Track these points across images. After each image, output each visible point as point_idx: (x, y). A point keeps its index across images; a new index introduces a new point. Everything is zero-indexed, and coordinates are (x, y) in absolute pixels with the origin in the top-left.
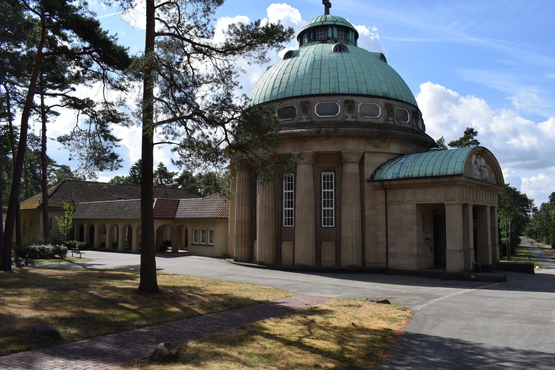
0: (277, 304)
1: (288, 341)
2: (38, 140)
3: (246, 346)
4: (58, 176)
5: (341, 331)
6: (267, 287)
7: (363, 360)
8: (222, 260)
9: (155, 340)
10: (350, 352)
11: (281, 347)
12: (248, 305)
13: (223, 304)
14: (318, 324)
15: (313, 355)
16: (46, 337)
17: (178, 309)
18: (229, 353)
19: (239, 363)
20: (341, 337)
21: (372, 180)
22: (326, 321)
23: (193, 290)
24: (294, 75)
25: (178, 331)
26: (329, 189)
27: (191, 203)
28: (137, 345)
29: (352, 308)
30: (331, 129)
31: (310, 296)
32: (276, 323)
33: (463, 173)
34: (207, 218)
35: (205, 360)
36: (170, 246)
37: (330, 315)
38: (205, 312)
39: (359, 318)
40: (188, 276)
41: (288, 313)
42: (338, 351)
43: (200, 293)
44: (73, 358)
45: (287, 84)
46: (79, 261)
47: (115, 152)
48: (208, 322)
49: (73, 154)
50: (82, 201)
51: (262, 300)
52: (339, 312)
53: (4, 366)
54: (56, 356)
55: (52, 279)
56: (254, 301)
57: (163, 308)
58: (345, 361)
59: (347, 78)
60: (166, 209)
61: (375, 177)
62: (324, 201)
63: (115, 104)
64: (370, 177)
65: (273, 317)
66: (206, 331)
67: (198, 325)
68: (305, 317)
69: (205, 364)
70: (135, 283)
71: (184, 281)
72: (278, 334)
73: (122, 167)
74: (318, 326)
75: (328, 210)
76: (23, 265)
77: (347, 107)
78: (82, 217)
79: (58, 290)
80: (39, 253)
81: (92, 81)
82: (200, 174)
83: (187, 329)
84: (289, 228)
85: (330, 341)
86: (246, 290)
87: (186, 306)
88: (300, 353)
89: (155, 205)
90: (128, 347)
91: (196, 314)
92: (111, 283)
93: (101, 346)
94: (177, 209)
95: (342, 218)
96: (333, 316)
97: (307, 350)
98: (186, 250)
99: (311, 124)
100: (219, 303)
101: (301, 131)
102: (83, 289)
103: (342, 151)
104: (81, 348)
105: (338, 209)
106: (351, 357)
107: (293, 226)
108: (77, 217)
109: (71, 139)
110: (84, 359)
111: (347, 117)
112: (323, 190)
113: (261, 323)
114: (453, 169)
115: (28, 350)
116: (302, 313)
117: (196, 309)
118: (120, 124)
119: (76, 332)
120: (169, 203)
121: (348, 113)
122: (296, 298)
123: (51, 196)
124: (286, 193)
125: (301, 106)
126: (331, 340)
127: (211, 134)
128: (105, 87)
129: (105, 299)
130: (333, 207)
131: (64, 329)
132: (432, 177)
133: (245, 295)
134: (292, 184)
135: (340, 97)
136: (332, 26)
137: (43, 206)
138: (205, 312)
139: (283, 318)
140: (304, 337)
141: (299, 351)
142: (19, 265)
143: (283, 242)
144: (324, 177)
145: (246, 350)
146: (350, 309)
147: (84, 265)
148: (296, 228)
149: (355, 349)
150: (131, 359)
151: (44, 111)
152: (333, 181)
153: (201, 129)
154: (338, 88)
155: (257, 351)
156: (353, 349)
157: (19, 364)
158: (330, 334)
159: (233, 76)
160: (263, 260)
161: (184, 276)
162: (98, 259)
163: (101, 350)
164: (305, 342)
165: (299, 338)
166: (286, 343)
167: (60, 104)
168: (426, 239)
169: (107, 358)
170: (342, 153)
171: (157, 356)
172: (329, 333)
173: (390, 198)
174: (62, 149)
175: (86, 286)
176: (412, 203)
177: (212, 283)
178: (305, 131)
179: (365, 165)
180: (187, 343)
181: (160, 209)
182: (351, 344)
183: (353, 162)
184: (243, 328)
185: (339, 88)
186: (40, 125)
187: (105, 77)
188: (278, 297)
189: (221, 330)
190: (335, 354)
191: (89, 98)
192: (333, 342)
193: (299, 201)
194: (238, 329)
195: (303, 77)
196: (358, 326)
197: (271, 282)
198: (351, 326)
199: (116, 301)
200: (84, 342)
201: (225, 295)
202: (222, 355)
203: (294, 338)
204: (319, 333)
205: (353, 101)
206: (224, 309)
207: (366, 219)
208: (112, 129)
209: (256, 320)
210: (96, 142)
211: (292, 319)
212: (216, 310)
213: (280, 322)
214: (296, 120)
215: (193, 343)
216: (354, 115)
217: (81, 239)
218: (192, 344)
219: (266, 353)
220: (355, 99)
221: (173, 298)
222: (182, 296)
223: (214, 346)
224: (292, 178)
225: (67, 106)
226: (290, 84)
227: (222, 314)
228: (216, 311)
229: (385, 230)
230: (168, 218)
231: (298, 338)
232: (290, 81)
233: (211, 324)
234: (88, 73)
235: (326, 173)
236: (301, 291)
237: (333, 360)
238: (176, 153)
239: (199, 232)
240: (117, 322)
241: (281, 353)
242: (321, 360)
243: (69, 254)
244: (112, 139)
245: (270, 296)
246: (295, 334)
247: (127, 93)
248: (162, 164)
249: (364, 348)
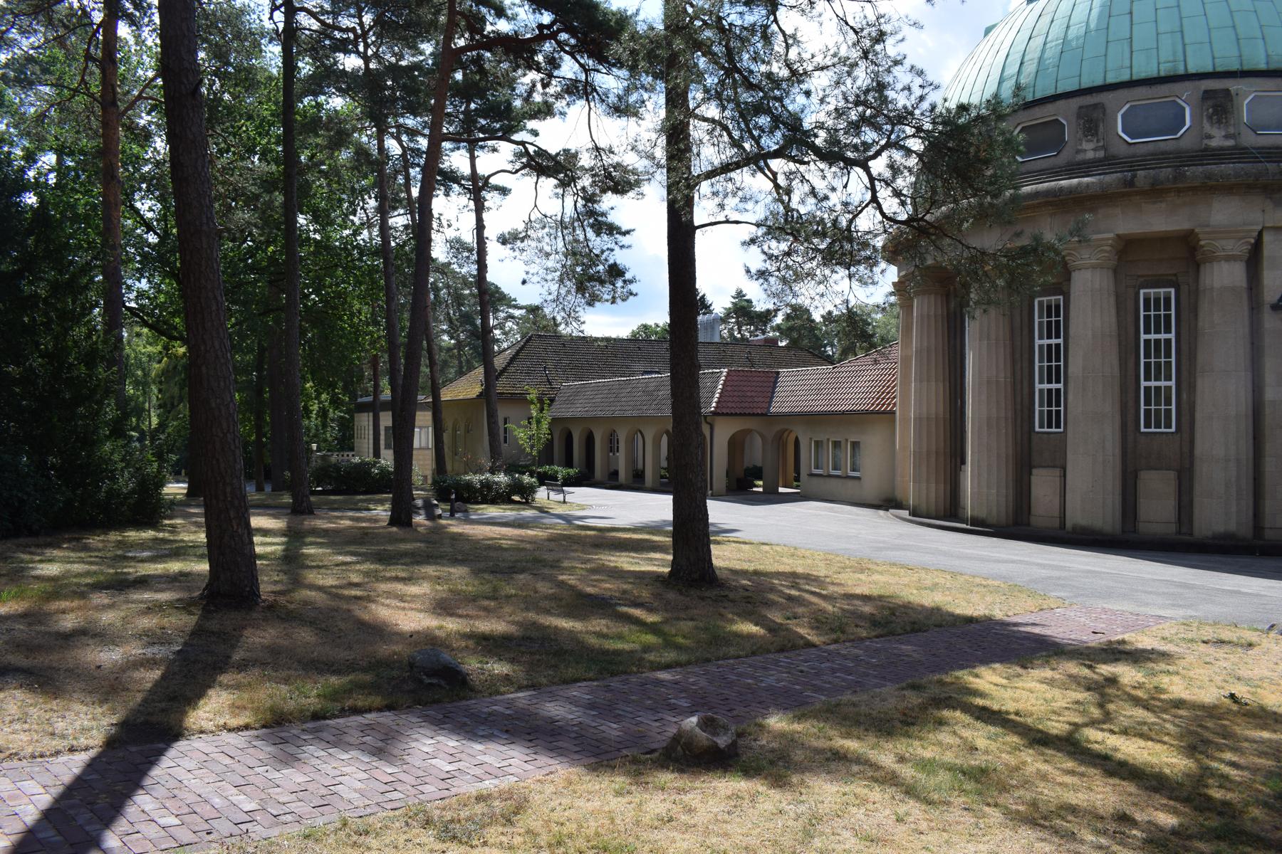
0: (1015, 628)
1: (1040, 735)
2: (470, 250)
3: (921, 739)
4: (520, 328)
5: (1197, 716)
6: (990, 582)
7: (1266, 810)
8: (881, 512)
9: (686, 705)
10: (1224, 781)
11: (1017, 748)
12: (936, 626)
13: (873, 622)
14: (1128, 689)
15: (1112, 781)
16: (434, 681)
17: (758, 628)
18: (873, 755)
19: (894, 788)
20: (1197, 733)
22: (1151, 683)
23: (801, 581)
24: (1057, 40)
25: (749, 684)
27: (806, 377)
28: (641, 713)
29: (1227, 648)
30: (1166, 173)
31: (1105, 611)
32: (1008, 678)
34: (843, 413)
35: (802, 769)
36: (760, 479)
37: (1163, 666)
38: (822, 639)
39: (1250, 679)
40: (796, 549)
41: (1044, 653)
42: (1188, 775)
43: (817, 590)
44: (482, 736)
45: (1039, 63)
46: (560, 510)
47: (618, 262)
48: (828, 664)
49: (531, 271)
50: (567, 381)
51: (976, 614)
52: (1190, 658)
53: (324, 743)
54: (444, 729)
55: (489, 547)
56: (952, 615)
57: (721, 623)
58: (1209, 809)
60: (749, 394)
62: (1147, 318)
63: (616, 150)
65: (1001, 662)
66: (818, 689)
67: (802, 671)
68: (1090, 667)
69: (802, 782)
70: (660, 563)
71: (785, 560)
72: (1012, 710)
73: (636, 295)
74: (1129, 695)
75: (1158, 389)
76: (440, 517)
77: (1211, 110)
78: (569, 415)
79: (492, 572)
80: (480, 490)
81: (564, 102)
82: (830, 313)
83: (771, 681)
85: (1165, 743)
86: (934, 587)
87: (779, 621)
88: (1071, 772)
89: (723, 385)
90: (618, 718)
91: (802, 642)
92: (612, 558)
93: (555, 709)
94: (773, 392)
95: (1198, 408)
96: (1171, 668)
97: (1095, 766)
98: (797, 487)
99: (1107, 163)
100: (861, 616)
101: (1079, 184)
102: (546, 571)
103: (1197, 230)
104: (508, 712)
105: (1187, 384)
106: (1228, 797)
107: (1062, 430)
108: (559, 415)
109: (525, 237)
110: (505, 742)
111: (1210, 137)
112: (1143, 337)
113: (966, 677)
115: (390, 708)
116: (1081, 654)
117: (801, 631)
118: (631, 194)
119: (506, 672)
120: (755, 379)
121: (1212, 124)
122: (1068, 613)
123: (504, 370)
125: (1079, 116)
126: (1166, 739)
127: (833, 189)
128: (592, 113)
129: (590, 595)
130: (1171, 380)
131: (481, 662)
133: (930, 600)
134: (1058, 323)
135: (1187, 84)
137: (487, 395)
138: (822, 639)
139: (1029, 665)
140: (1086, 725)
141: (1070, 764)
142: (431, 516)
143: (1035, 471)
144: (1147, 301)
145: (920, 751)
146: (1220, 652)
147: (567, 519)
148: (1070, 435)
149: (1240, 773)
151: (478, 187)
152: (1173, 312)
153: (808, 181)
154: (1182, 59)
155: (949, 757)
156: (1233, 772)
157: (358, 741)
158: (1165, 720)
159: (890, 41)
160: (982, 513)
161: (786, 549)
162: (600, 506)
163: (552, 721)
164: (1088, 741)
165: (1071, 727)
166: (1034, 739)
167: (509, 167)
169: (560, 744)
170: (1197, 234)
171: (679, 748)
172: (1159, 717)
174: (507, 261)
175: (555, 565)
177: (851, 567)
178: (1093, 183)
179: (1265, 263)
180: (764, 718)
181: (736, 393)
182: (1228, 756)
183: (1230, 258)
184: (915, 687)
185: (1185, 61)
186: (472, 217)
187: (589, 89)
188: (1018, 610)
189: (858, 689)
190: (1178, 783)
191: (569, 150)
192: (1172, 745)
193: (1076, 365)
194: (903, 689)
195: (1081, 41)
196: (1246, 704)
197: (1003, 569)
198: (1228, 701)
199: (613, 602)
200: (519, 698)
201: (880, 598)
202: (851, 761)
203: (1056, 725)
204: (1131, 717)
205: (1227, 92)
206: (874, 634)
208: (612, 208)
209: (952, 669)
210: (577, 241)
211: (1053, 669)
212: (852, 634)
213: (1019, 676)
214: (1066, 156)
215: (781, 720)
216: (1231, 130)
217: (569, 463)
218: (777, 722)
219: (973, 762)
221: (748, 600)
222: (772, 596)
223: (832, 733)
224: (1058, 307)
225: (523, 172)
226: (1047, 62)
227: (867, 646)
228: (852, 637)
230: (754, 415)
231: (1067, 726)
232: (1046, 56)
233: (833, 671)
234: (554, 82)
235: (1152, 291)
236: (1082, 595)
237: (1172, 803)
238: (754, 248)
239: (825, 446)
240: (606, 652)
241: (1017, 769)
242: (1136, 800)
243: (542, 494)
244: (612, 229)
245: (998, 606)
246: (1059, 715)
247: (640, 122)
248: (741, 291)
249: (1270, 774)
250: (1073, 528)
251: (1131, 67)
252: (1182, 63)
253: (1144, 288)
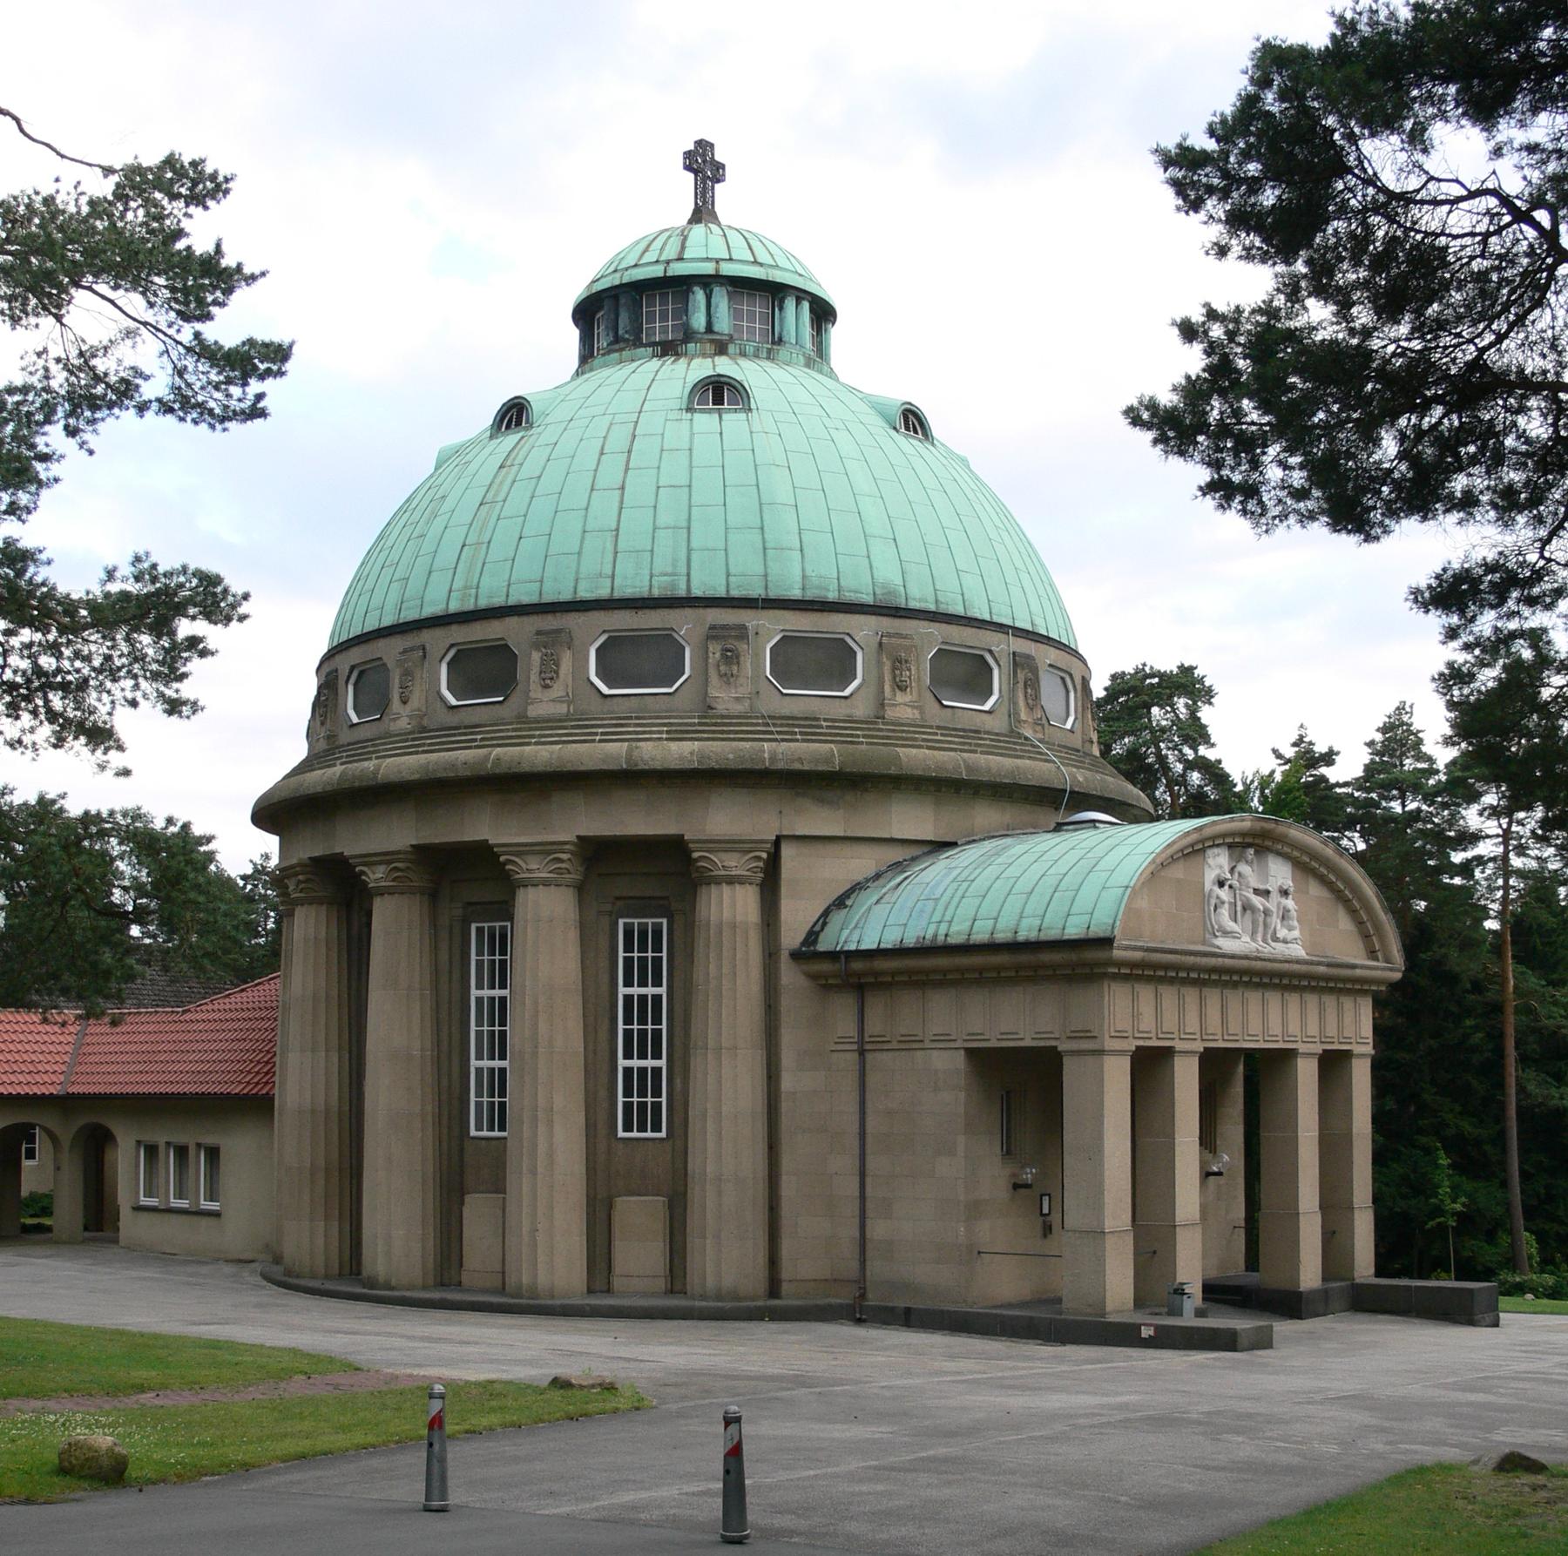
21: (806, 954)
26: (647, 986)
33: (1116, 933)
59: (761, 504)
61: (822, 937)
62: (628, 962)
64: (800, 937)
84: (494, 1142)
112: (623, 991)
114: (1087, 917)
124: (479, 1000)
132: (1014, 947)
135: (688, 612)
136: (707, 282)
143: (468, 1198)
154: (684, 571)
168: (1016, 1186)
173: (874, 1026)
176: (952, 1045)
185: (688, 575)
205: (742, 628)
207: (785, 1106)
229: (857, 1151)
250: (31, 1193)
251: (613, 577)
252: (685, 578)
253: (622, 917)
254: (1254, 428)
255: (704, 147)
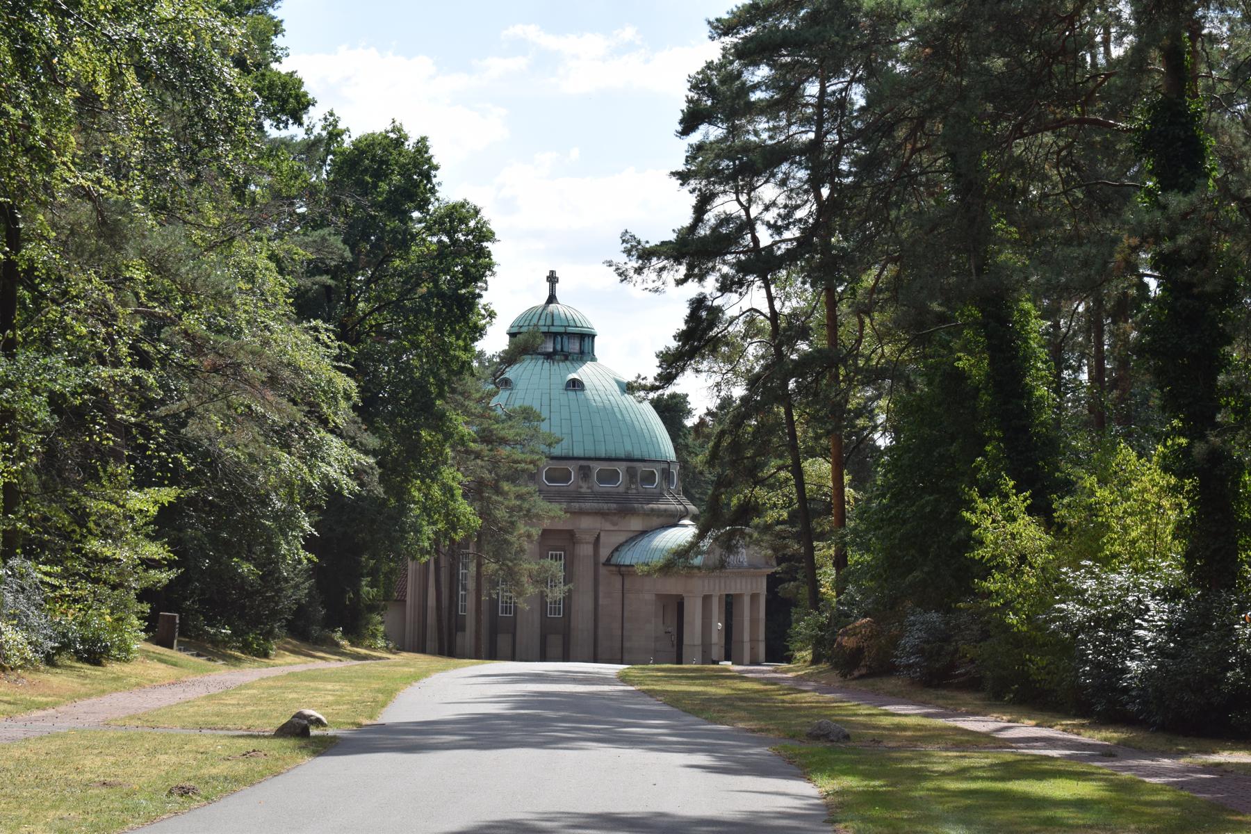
21: (608, 563)
111: (581, 487)
150: (238, 704)
173: (627, 586)
179: (601, 545)
205: (589, 467)
220: (591, 464)
254: (837, 768)
255: (552, 272)
